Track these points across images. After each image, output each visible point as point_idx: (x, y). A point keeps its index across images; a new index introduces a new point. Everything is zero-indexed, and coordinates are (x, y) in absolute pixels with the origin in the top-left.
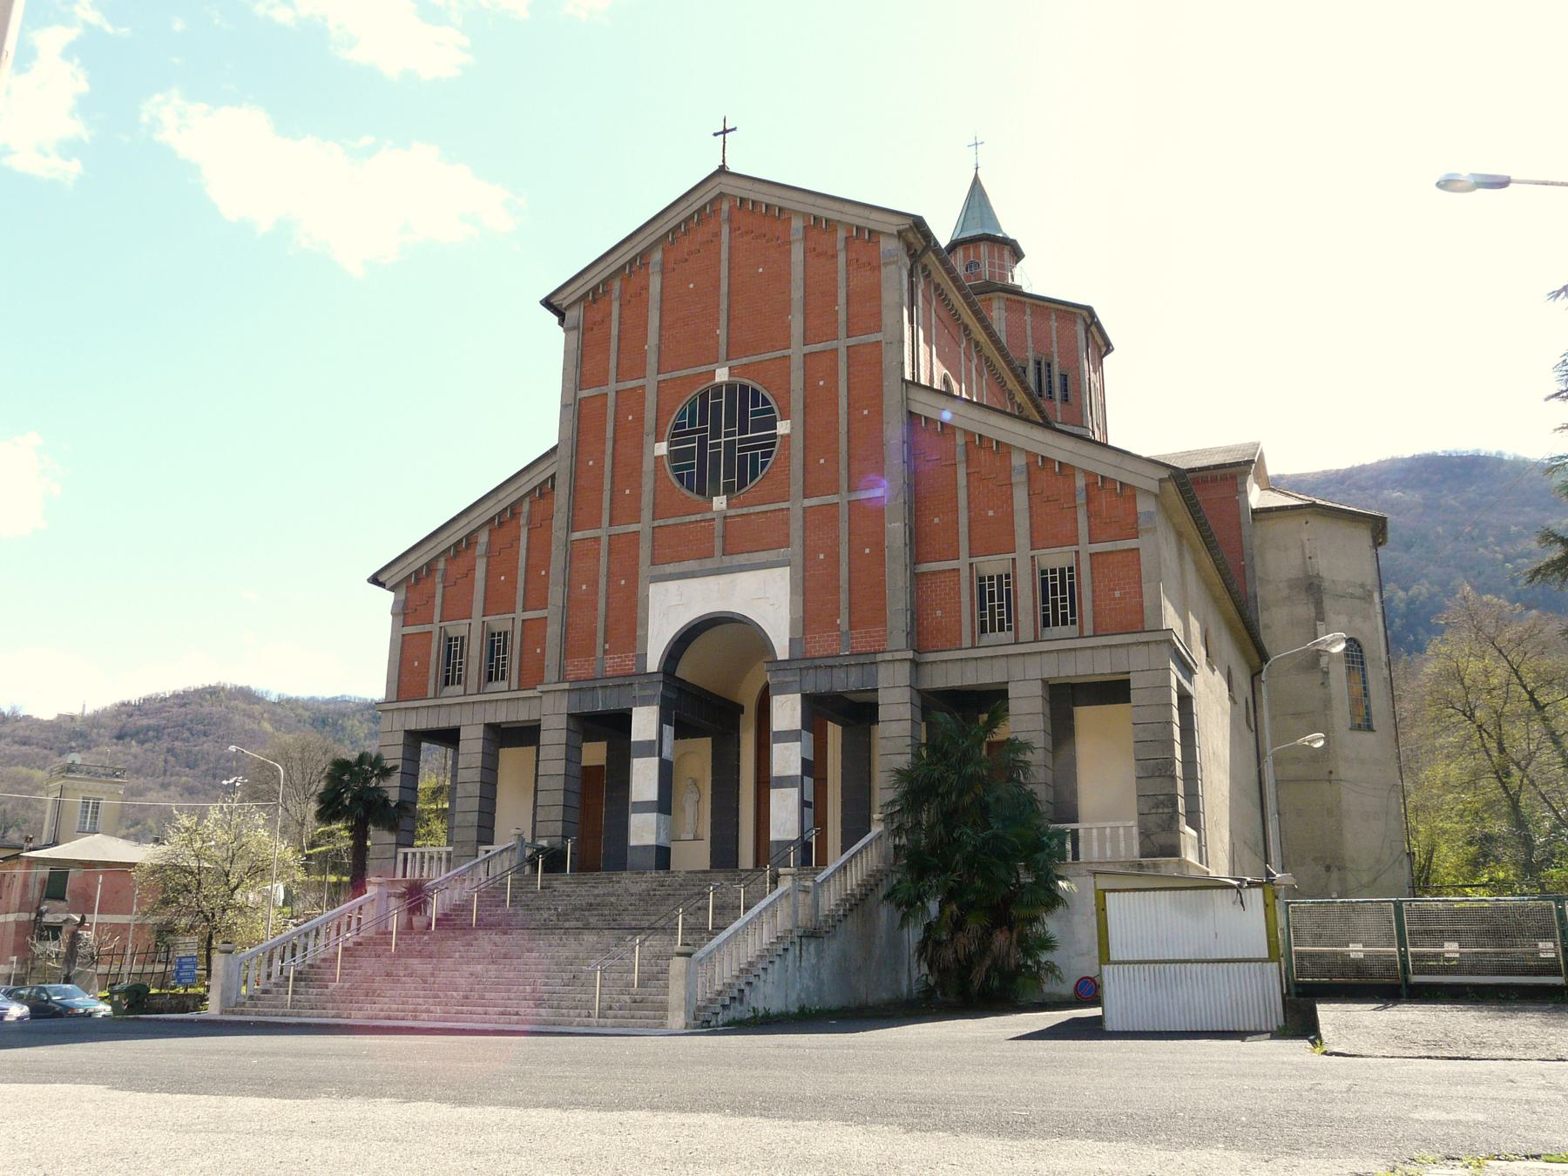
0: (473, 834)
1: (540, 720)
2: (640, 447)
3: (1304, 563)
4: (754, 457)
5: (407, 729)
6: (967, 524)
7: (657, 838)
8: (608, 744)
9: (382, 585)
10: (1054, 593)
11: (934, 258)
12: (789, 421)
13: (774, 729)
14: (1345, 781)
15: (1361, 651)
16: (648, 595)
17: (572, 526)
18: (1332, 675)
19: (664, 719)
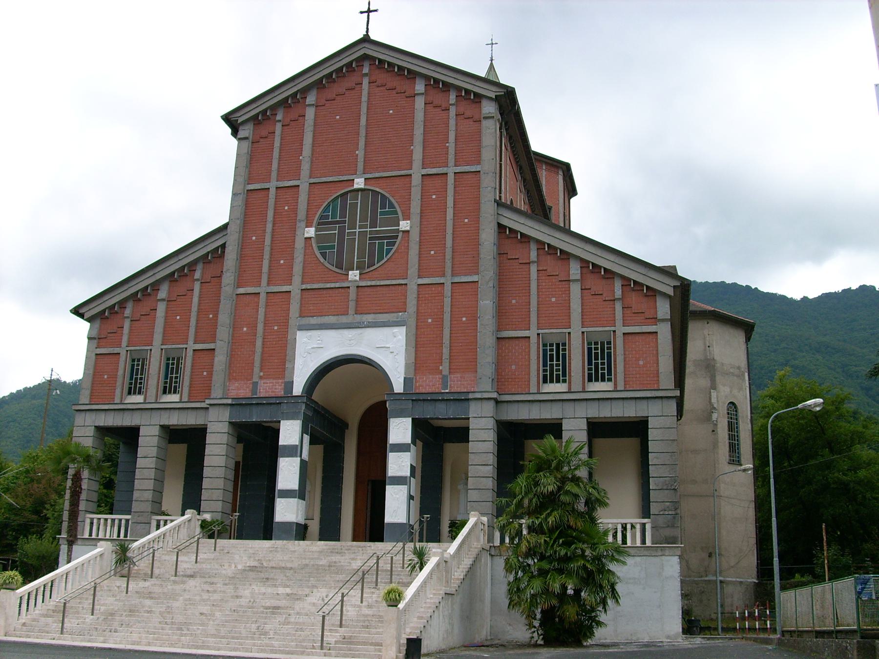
0: (148, 507)
1: (207, 425)
2: (293, 230)
3: (705, 350)
4: (381, 246)
5: (97, 425)
6: (536, 306)
7: (297, 517)
8: (324, 447)
9: (81, 316)
10: (596, 359)
11: (513, 118)
12: (409, 222)
13: (390, 442)
14: (724, 497)
15: (736, 411)
16: (295, 339)
17: (239, 284)
18: (719, 426)
19: (304, 430)
